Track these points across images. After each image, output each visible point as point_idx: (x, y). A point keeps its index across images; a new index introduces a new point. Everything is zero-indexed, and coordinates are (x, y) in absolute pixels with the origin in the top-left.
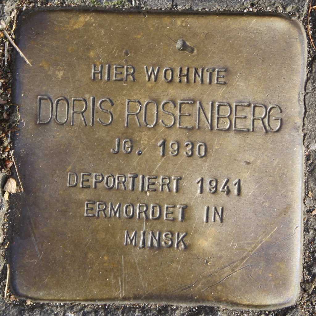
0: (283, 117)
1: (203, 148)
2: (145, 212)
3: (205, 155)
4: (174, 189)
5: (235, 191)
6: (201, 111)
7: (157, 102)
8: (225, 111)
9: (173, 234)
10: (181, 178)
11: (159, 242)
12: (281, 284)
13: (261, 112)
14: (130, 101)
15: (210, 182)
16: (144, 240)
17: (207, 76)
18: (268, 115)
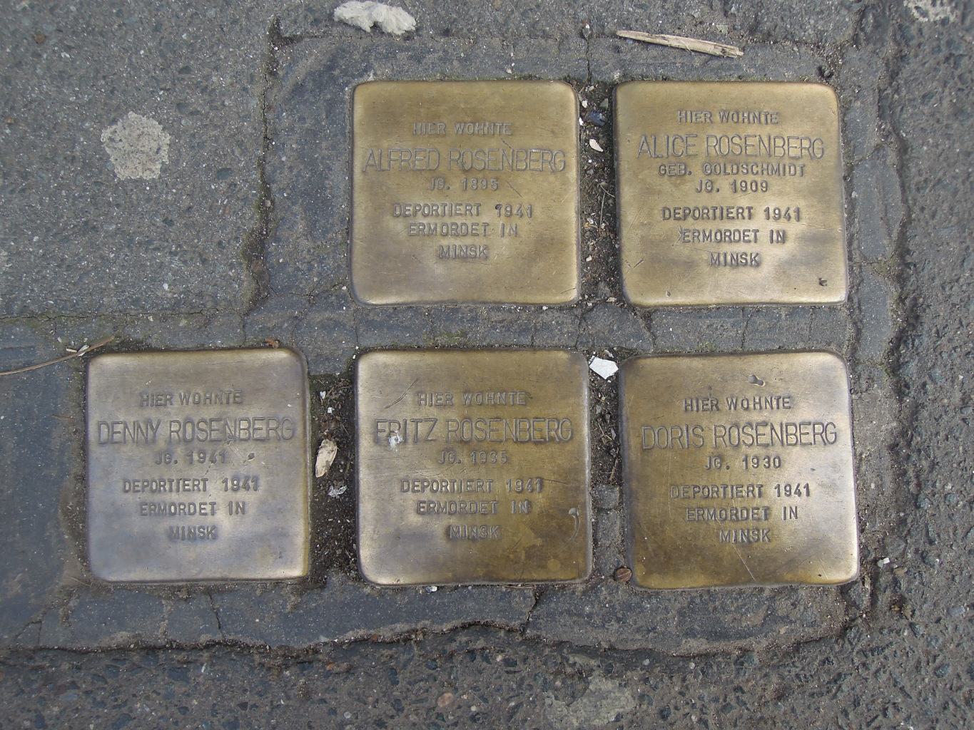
0: (247, 501)
1: (777, 460)
2: (716, 405)
3: (779, 466)
4: (757, 495)
5: (804, 491)
6: (774, 433)
7: (737, 425)
8: (792, 429)
9: (758, 531)
10: (762, 486)
11: (748, 538)
12: (566, 292)
13: (819, 428)
14: (603, 34)
15: (785, 487)
16: (736, 537)
17: (775, 403)
18: (825, 429)
